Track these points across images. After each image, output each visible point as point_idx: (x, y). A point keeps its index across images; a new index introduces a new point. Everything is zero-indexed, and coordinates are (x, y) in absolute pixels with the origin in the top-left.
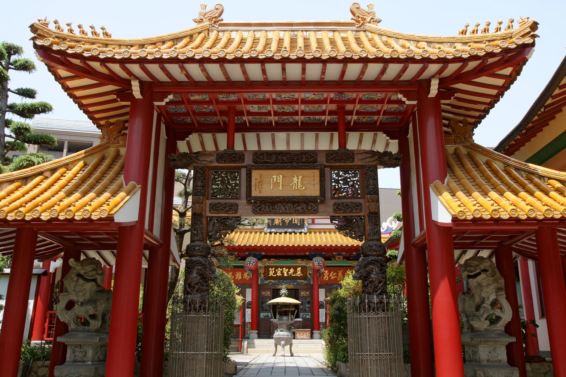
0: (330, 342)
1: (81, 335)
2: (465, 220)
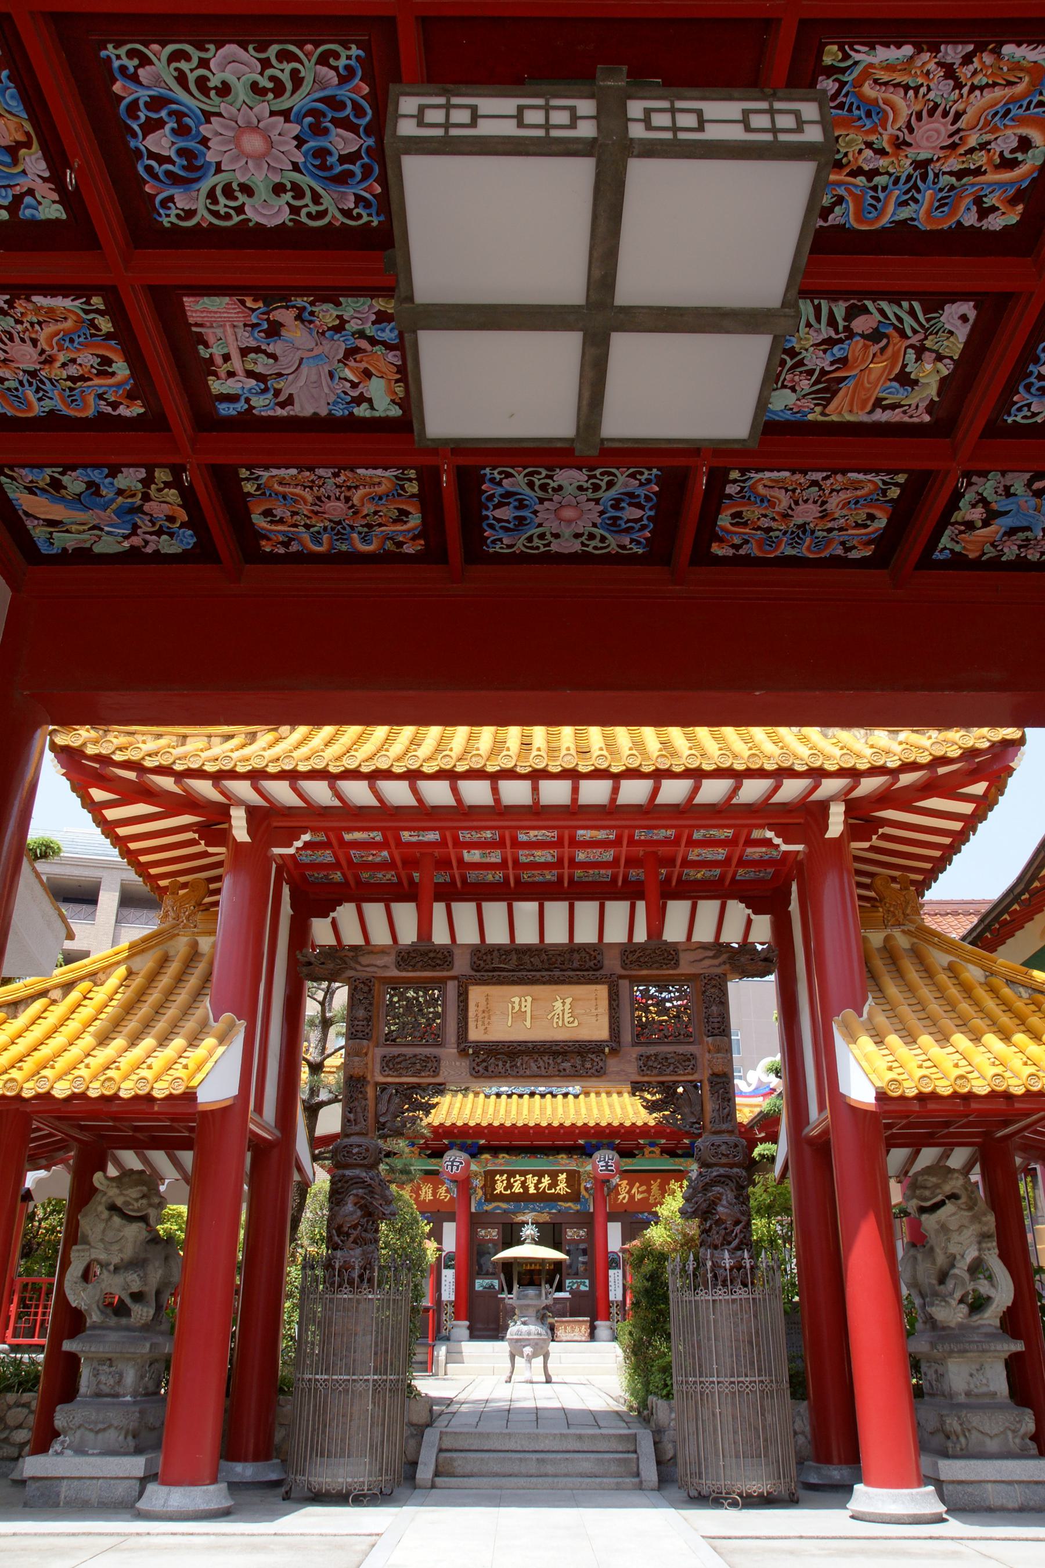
0: (635, 1353)
1: (113, 1336)
2: (902, 1098)
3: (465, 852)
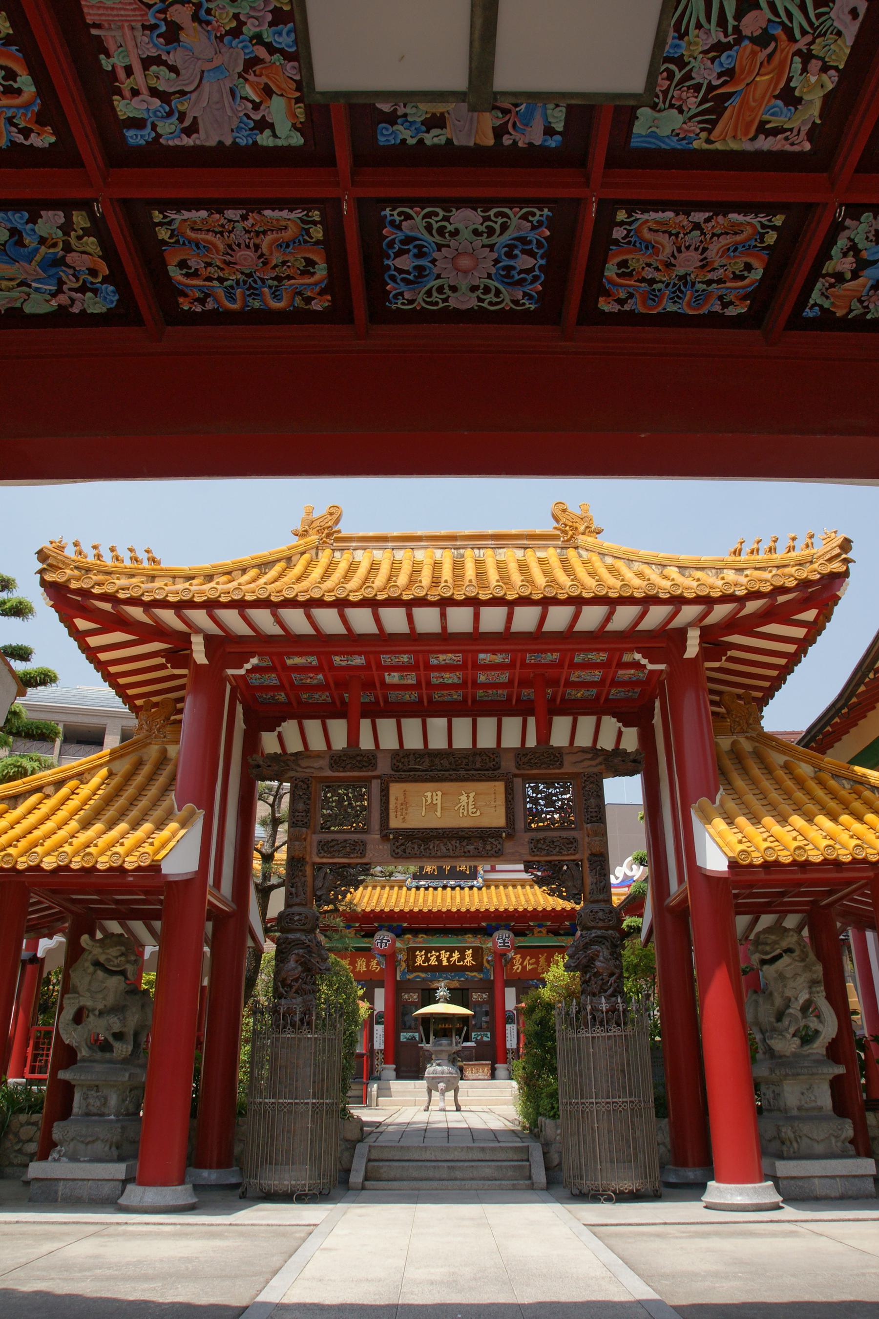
1: (98, 1067)
2: (751, 865)
3: (386, 674)
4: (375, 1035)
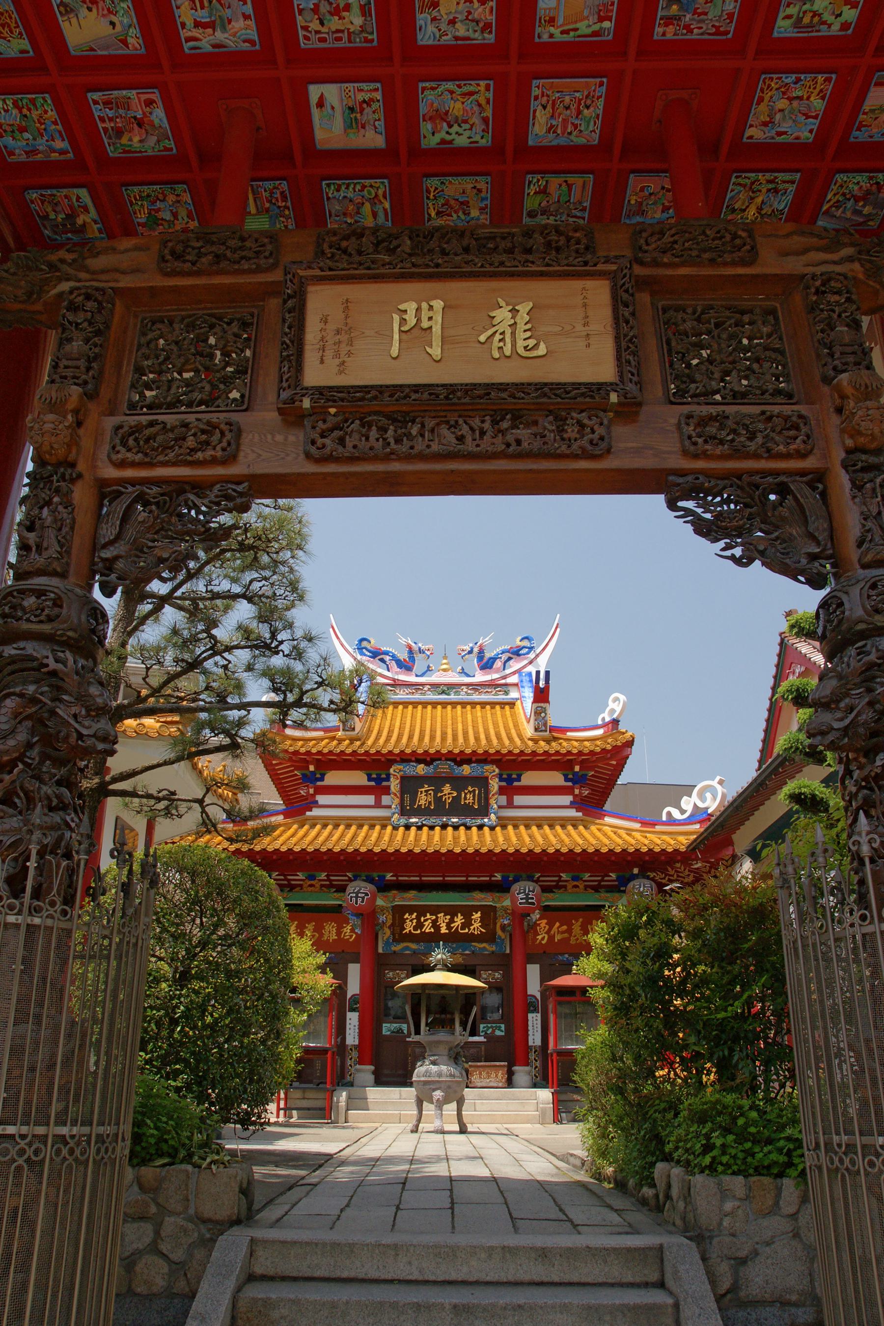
4: (348, 1026)
